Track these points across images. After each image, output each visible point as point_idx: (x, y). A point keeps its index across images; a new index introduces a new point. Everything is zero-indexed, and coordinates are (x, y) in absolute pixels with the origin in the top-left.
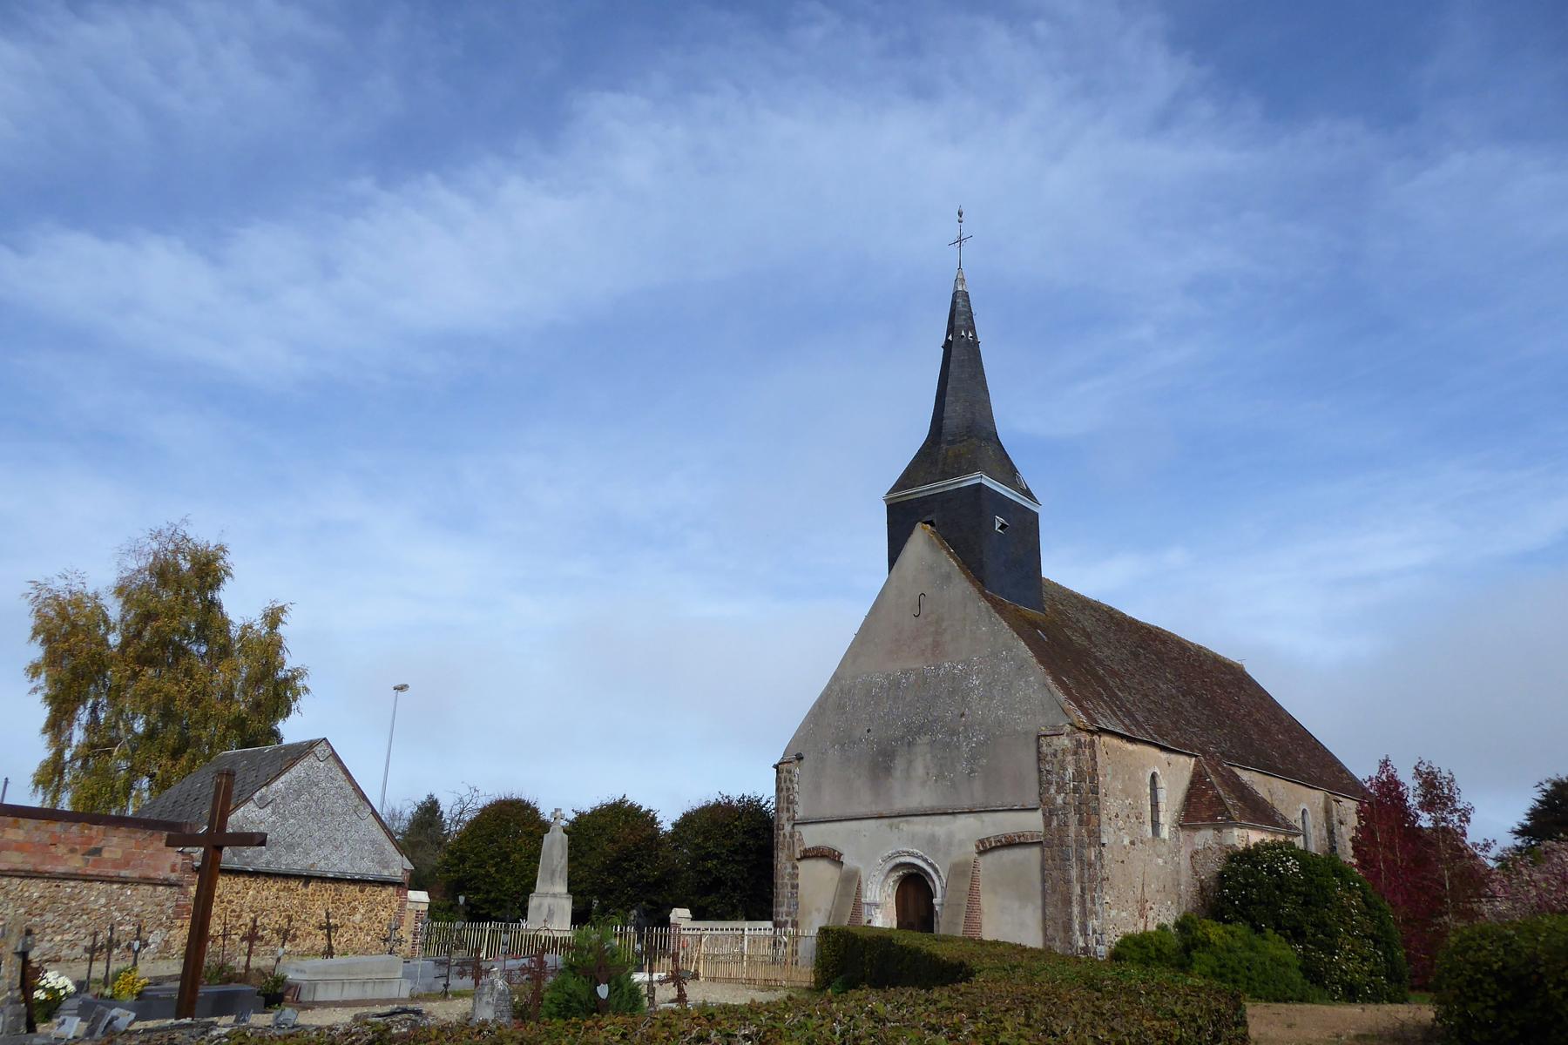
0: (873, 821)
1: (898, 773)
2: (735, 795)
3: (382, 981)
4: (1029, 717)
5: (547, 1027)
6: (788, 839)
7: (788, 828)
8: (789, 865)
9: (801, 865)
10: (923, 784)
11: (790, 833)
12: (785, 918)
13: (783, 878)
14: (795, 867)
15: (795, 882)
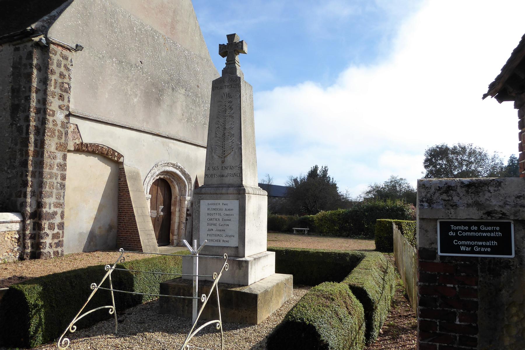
0: (151, 136)
1: (165, 106)
2: (503, 66)
3: (238, 62)
4: (4, 119)
5: (6, 250)
6: (59, 127)
7: (60, 116)
8: (59, 155)
9: (70, 156)
10: (180, 121)
11: (63, 123)
12: (53, 209)
13: (51, 167)
14: (65, 158)
15: (64, 173)
